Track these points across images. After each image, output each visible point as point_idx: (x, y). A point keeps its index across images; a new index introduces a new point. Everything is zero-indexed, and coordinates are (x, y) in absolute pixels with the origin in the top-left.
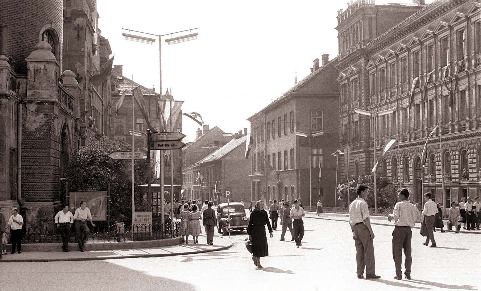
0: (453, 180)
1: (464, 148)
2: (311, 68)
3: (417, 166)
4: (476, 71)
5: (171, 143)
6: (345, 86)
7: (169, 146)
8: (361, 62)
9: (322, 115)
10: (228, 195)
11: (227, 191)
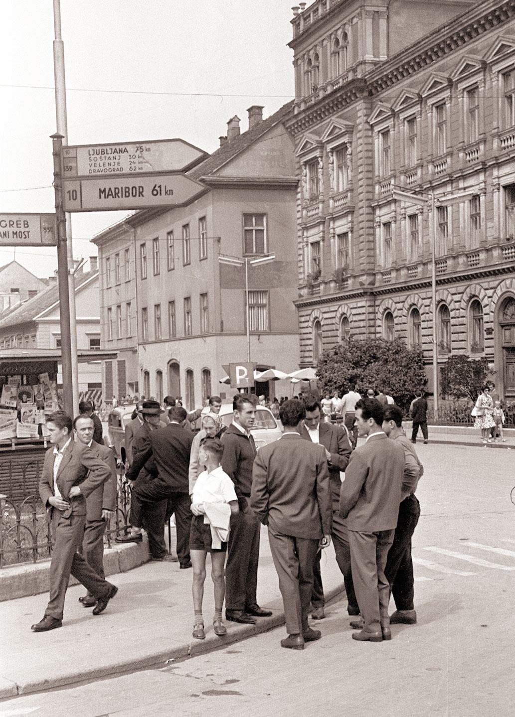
7: (141, 193)
8: (355, 107)
10: (241, 380)
11: (238, 368)
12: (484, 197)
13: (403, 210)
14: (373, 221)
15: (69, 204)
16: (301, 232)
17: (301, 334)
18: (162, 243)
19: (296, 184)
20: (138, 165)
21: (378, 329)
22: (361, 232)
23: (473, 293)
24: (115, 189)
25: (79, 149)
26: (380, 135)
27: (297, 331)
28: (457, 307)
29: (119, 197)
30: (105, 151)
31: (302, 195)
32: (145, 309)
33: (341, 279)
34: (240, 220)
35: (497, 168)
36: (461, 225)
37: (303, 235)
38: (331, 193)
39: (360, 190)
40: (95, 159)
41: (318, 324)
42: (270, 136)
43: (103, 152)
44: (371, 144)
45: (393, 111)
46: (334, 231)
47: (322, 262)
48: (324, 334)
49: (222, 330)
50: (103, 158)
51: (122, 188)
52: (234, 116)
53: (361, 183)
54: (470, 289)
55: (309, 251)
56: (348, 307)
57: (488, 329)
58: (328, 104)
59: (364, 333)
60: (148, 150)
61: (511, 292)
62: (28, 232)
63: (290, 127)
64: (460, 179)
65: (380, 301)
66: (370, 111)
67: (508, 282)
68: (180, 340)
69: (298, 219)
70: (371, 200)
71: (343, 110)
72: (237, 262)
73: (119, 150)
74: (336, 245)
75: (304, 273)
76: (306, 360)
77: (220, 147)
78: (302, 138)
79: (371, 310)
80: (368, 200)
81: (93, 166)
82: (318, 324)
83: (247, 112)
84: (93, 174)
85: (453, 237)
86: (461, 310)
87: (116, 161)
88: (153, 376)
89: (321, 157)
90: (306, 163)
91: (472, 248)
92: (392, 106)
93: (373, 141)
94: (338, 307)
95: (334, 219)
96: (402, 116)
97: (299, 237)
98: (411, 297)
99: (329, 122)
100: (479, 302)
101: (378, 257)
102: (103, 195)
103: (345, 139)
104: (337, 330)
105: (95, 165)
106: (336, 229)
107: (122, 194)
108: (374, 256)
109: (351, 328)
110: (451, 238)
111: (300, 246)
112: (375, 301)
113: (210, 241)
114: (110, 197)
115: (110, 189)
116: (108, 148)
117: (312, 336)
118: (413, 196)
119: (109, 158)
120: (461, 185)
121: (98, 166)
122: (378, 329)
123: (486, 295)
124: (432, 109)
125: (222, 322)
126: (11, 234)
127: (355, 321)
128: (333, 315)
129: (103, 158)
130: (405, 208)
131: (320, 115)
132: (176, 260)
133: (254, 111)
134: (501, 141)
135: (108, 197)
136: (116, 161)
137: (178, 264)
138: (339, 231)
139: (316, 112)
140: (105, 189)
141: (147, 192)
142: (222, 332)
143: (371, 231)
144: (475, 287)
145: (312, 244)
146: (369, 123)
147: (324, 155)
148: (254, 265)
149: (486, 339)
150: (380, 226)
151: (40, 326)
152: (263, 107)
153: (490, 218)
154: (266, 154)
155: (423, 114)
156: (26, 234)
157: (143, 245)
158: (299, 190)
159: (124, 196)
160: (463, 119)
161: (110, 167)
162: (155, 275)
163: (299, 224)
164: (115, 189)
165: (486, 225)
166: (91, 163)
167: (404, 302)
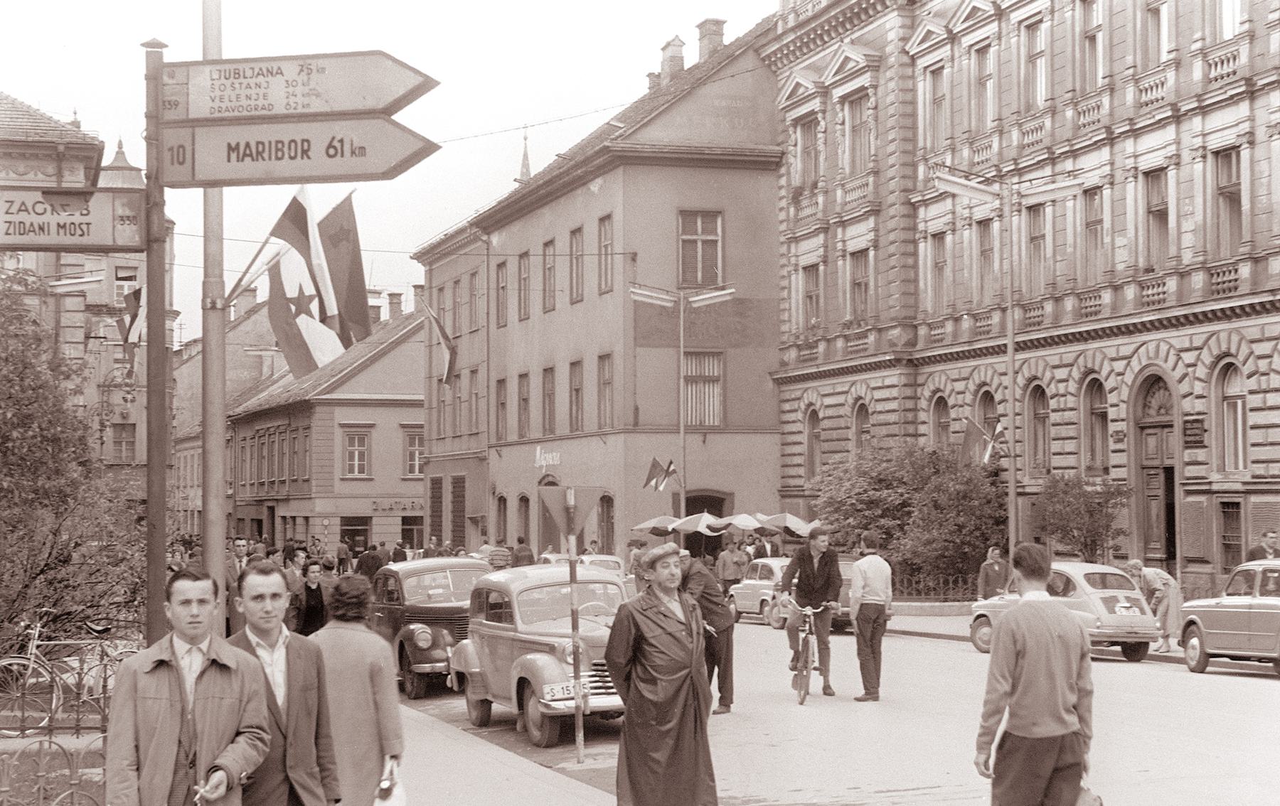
0: (1114, 473)
1: (1093, 371)
2: (650, 75)
3: (1145, 415)
4: (845, 218)
5: (319, 135)
6: (808, 122)
7: (305, 153)
9: (719, 231)
12: (1109, 191)
13: (967, 211)
14: (914, 228)
15: (172, 171)
16: (785, 247)
17: (784, 434)
18: (535, 261)
19: (778, 160)
20: (300, 99)
21: (922, 429)
22: (892, 249)
23: (1089, 365)
24: (258, 143)
25: (191, 69)
26: (928, 74)
27: (778, 426)
28: (1062, 391)
29: (263, 159)
30: (241, 73)
31: (789, 180)
32: (501, 382)
33: (855, 329)
34: (672, 223)
35: (1132, 139)
36: (1070, 240)
37: (789, 252)
38: (839, 177)
39: (891, 173)
40: (222, 87)
41: (814, 416)
42: (729, 71)
43: (237, 74)
44: (912, 90)
45: (950, 31)
46: (844, 246)
47: (822, 301)
48: (824, 435)
49: (636, 424)
50: (237, 86)
51: (270, 143)
52: (673, 37)
53: (891, 160)
54: (1085, 357)
55: (798, 282)
56: (868, 387)
57: (1117, 432)
58: (835, 17)
59: (896, 435)
60: (321, 70)
61: (1156, 365)
62: (88, 224)
63: (769, 56)
64: (1066, 158)
65: (925, 376)
66: (910, 31)
67: (1152, 346)
68: (561, 439)
69: (781, 222)
70: (911, 191)
71: (863, 28)
72: (665, 300)
73: (268, 70)
74: (848, 273)
75: (790, 321)
76: (792, 482)
77: (648, 91)
78: (789, 77)
79: (909, 392)
80: (905, 191)
81: (217, 100)
82: (814, 416)
83: (697, 30)
84: (217, 115)
85: (1056, 262)
86: (1069, 397)
87: (261, 91)
88: (513, 504)
89: (824, 112)
90: (796, 122)
91: (1089, 284)
92: (949, 23)
93: (915, 85)
94: (849, 384)
95: (843, 224)
96: (967, 41)
97: (782, 255)
98: (979, 372)
99: (836, 51)
100: (1101, 384)
101: (922, 296)
102: (234, 156)
103: (865, 80)
104: (848, 428)
105: (221, 99)
106: (848, 243)
107: (270, 154)
108: (916, 294)
109: (873, 425)
110: (1052, 262)
111: (785, 272)
112: (916, 375)
113: (619, 259)
114: (248, 159)
115: (248, 145)
116: (247, 66)
117: (803, 438)
118: (982, 187)
119: (249, 86)
120: (1068, 165)
121: (226, 99)
122: (922, 429)
123: (1112, 371)
124: (1019, 31)
125: (637, 409)
126: (54, 228)
127: (880, 412)
128: (841, 399)
129: (237, 86)
130: (971, 208)
131: (821, 36)
132: (557, 293)
133: (711, 28)
134: (1141, 91)
135: (243, 160)
136: (261, 91)
137: (562, 300)
138: (853, 246)
139: (814, 30)
140: (238, 144)
141: (318, 149)
142: (635, 426)
143: (910, 248)
144: (1094, 354)
145: (805, 268)
146: (908, 53)
147: (829, 108)
148: (695, 305)
149: (1114, 451)
150: (925, 238)
151: (318, 409)
152: (724, 22)
153: (1117, 230)
154: (724, 104)
155: (1003, 39)
156: (84, 227)
157: (501, 266)
158: (783, 170)
159: (273, 157)
160: (1074, 50)
161: (249, 102)
162: (521, 320)
163: (781, 232)
164: (258, 143)
165: (1113, 240)
166: (212, 95)
167: (967, 379)
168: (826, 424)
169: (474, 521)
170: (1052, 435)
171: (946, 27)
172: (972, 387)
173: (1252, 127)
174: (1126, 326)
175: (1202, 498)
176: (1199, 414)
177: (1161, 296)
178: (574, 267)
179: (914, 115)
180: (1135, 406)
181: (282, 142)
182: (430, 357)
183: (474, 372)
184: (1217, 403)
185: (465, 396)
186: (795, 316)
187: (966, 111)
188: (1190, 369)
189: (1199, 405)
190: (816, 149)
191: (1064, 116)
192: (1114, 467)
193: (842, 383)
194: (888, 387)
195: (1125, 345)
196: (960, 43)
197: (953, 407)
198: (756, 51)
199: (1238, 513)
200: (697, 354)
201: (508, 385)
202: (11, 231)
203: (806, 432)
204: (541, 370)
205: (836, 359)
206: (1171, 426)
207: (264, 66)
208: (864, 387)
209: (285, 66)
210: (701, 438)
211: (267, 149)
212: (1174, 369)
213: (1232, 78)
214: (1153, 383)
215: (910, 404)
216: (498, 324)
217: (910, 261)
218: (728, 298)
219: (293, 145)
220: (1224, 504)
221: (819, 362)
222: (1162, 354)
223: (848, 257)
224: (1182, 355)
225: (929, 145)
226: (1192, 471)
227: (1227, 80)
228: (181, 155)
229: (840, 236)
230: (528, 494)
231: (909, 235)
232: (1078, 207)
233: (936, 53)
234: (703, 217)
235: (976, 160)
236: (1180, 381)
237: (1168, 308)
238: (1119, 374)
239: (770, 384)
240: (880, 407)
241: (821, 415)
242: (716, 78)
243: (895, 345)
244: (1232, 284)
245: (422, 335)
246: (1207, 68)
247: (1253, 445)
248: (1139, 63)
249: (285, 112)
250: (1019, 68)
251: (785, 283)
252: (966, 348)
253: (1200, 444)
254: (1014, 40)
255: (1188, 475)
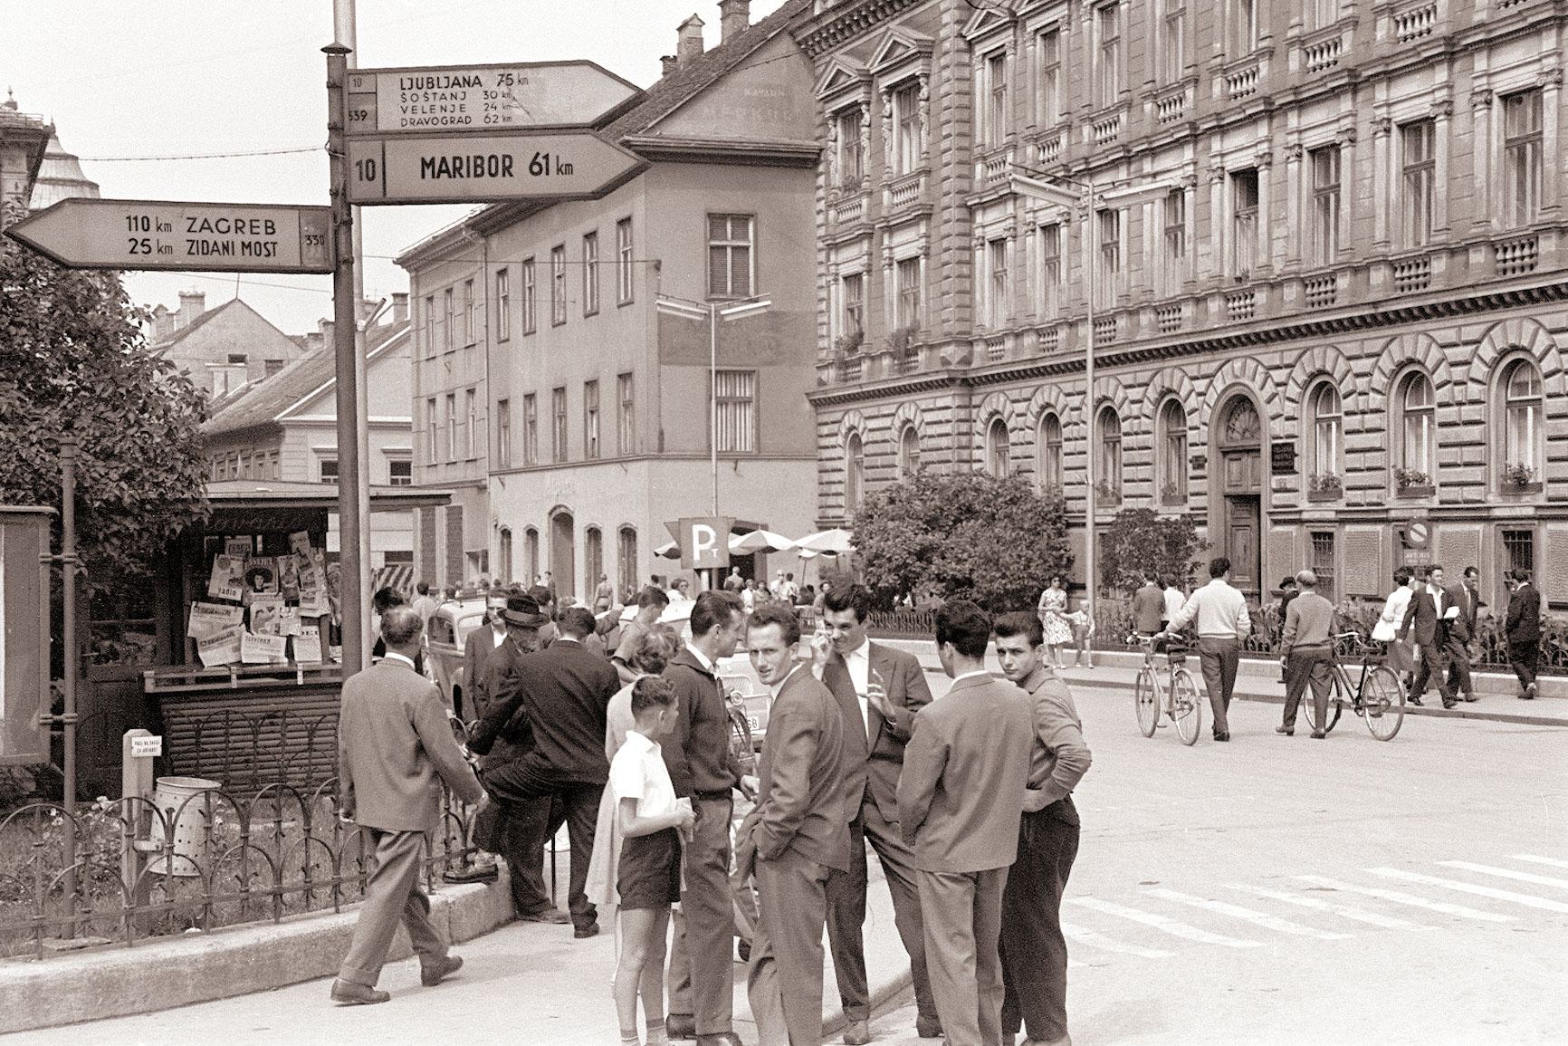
7: (507, 170)
13: (1031, 215)
20: (500, 112)
21: (977, 454)
24: (455, 159)
26: (987, 61)
27: (814, 453)
28: (1135, 413)
34: (700, 226)
38: (885, 177)
39: (945, 172)
41: (856, 442)
42: (765, 56)
43: (430, 82)
45: (1013, 14)
48: (867, 462)
49: (661, 449)
50: (431, 97)
52: (691, 15)
57: (1197, 458)
59: (948, 461)
62: (274, 243)
63: (806, 40)
68: (574, 466)
69: (819, 226)
72: (693, 312)
75: (829, 336)
76: (831, 512)
79: (963, 414)
82: (856, 442)
84: (409, 127)
88: (519, 539)
89: (868, 103)
95: (890, 230)
99: (885, 33)
102: (428, 172)
111: (823, 282)
112: (971, 396)
113: (640, 268)
114: (444, 176)
115: (444, 160)
116: (441, 75)
118: (1052, 187)
119: (443, 97)
120: (1148, 166)
121: (420, 111)
122: (977, 454)
125: (662, 433)
126: (238, 247)
127: (931, 436)
128: (886, 422)
129: (431, 97)
136: (457, 103)
137: (574, 313)
138: (901, 254)
140: (433, 159)
141: (521, 167)
148: (727, 319)
149: (1192, 478)
151: (288, 433)
156: (270, 247)
158: (821, 168)
161: (444, 114)
162: (525, 335)
164: (455, 159)
165: (1195, 249)
166: (404, 106)
168: (869, 449)
169: (473, 557)
170: (1124, 460)
171: (1009, 9)
172: (1035, 409)
173: (1355, 123)
174: (1209, 342)
175: (1292, 528)
176: (1288, 437)
177: (1249, 309)
178: (589, 276)
179: (970, 107)
180: (1217, 428)
181: (481, 158)
182: (418, 380)
183: (471, 392)
184: (1309, 426)
185: (440, 422)
186: (837, 328)
187: (1030, 102)
188: (1280, 389)
189: (1289, 427)
190: (859, 145)
191: (1143, 110)
192: (1192, 495)
193: (888, 405)
194: (940, 409)
195: (1207, 363)
196: (1024, 27)
197: (1013, 430)
198: (791, 34)
199: (1331, 545)
200: (727, 373)
201: (512, 405)
202: (194, 250)
203: (847, 457)
204: (551, 388)
205: (883, 378)
206: (1259, 450)
207: (460, 75)
208: (913, 408)
209: (486, 77)
210: (733, 465)
211: (465, 167)
212: (1262, 388)
213: (1333, 69)
214: (1239, 404)
215: (964, 427)
216: (499, 336)
217: (965, 270)
218: (764, 311)
219: (493, 161)
220: (1315, 535)
221: (861, 381)
222: (1249, 372)
223: (895, 266)
224: (1271, 372)
225: (987, 141)
226: (1279, 499)
227: (1326, 71)
228: (369, 170)
229: (886, 242)
230: (536, 526)
231: (964, 242)
232: (1156, 213)
233: (997, 38)
234: (733, 219)
235: (1041, 157)
236: (1269, 401)
237: (1257, 322)
238: (1200, 394)
239: (807, 406)
240: (932, 430)
241: (864, 439)
242: (748, 63)
243: (949, 363)
244: (1330, 295)
245: (407, 350)
246: (1304, 56)
247: (1067, 469)
248: (1227, 51)
249: (485, 125)
250: (1091, 57)
251: (823, 294)
252: (1029, 366)
253: (1289, 469)
254: (1086, 24)
255: (1275, 502)
